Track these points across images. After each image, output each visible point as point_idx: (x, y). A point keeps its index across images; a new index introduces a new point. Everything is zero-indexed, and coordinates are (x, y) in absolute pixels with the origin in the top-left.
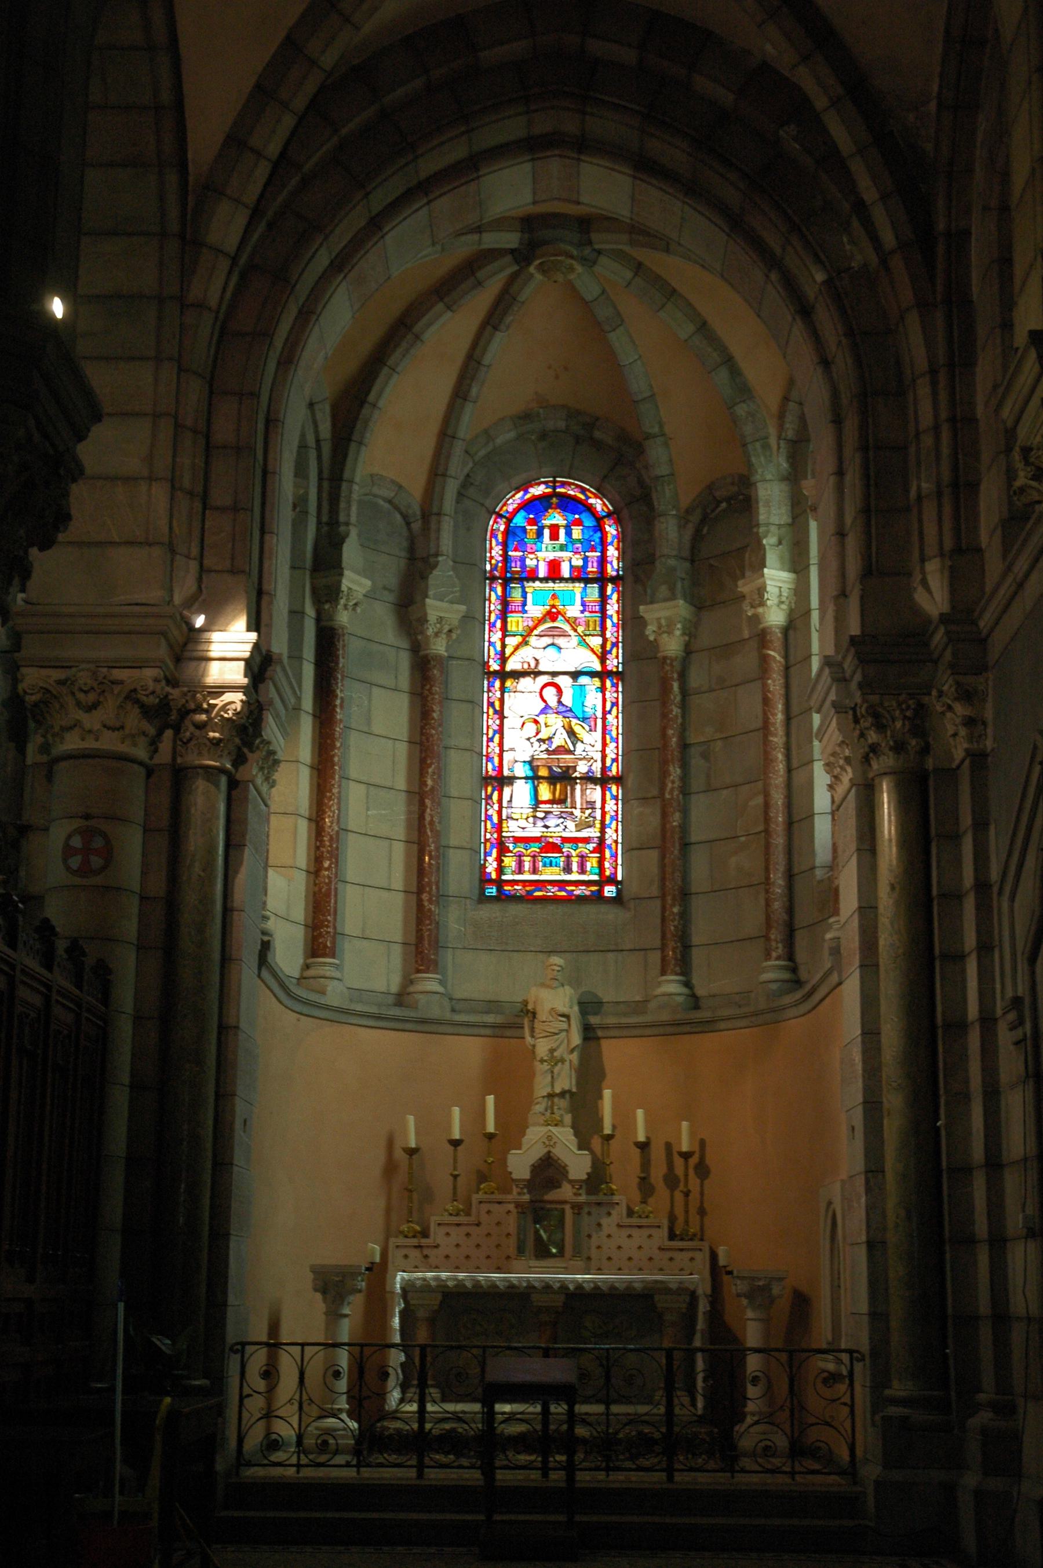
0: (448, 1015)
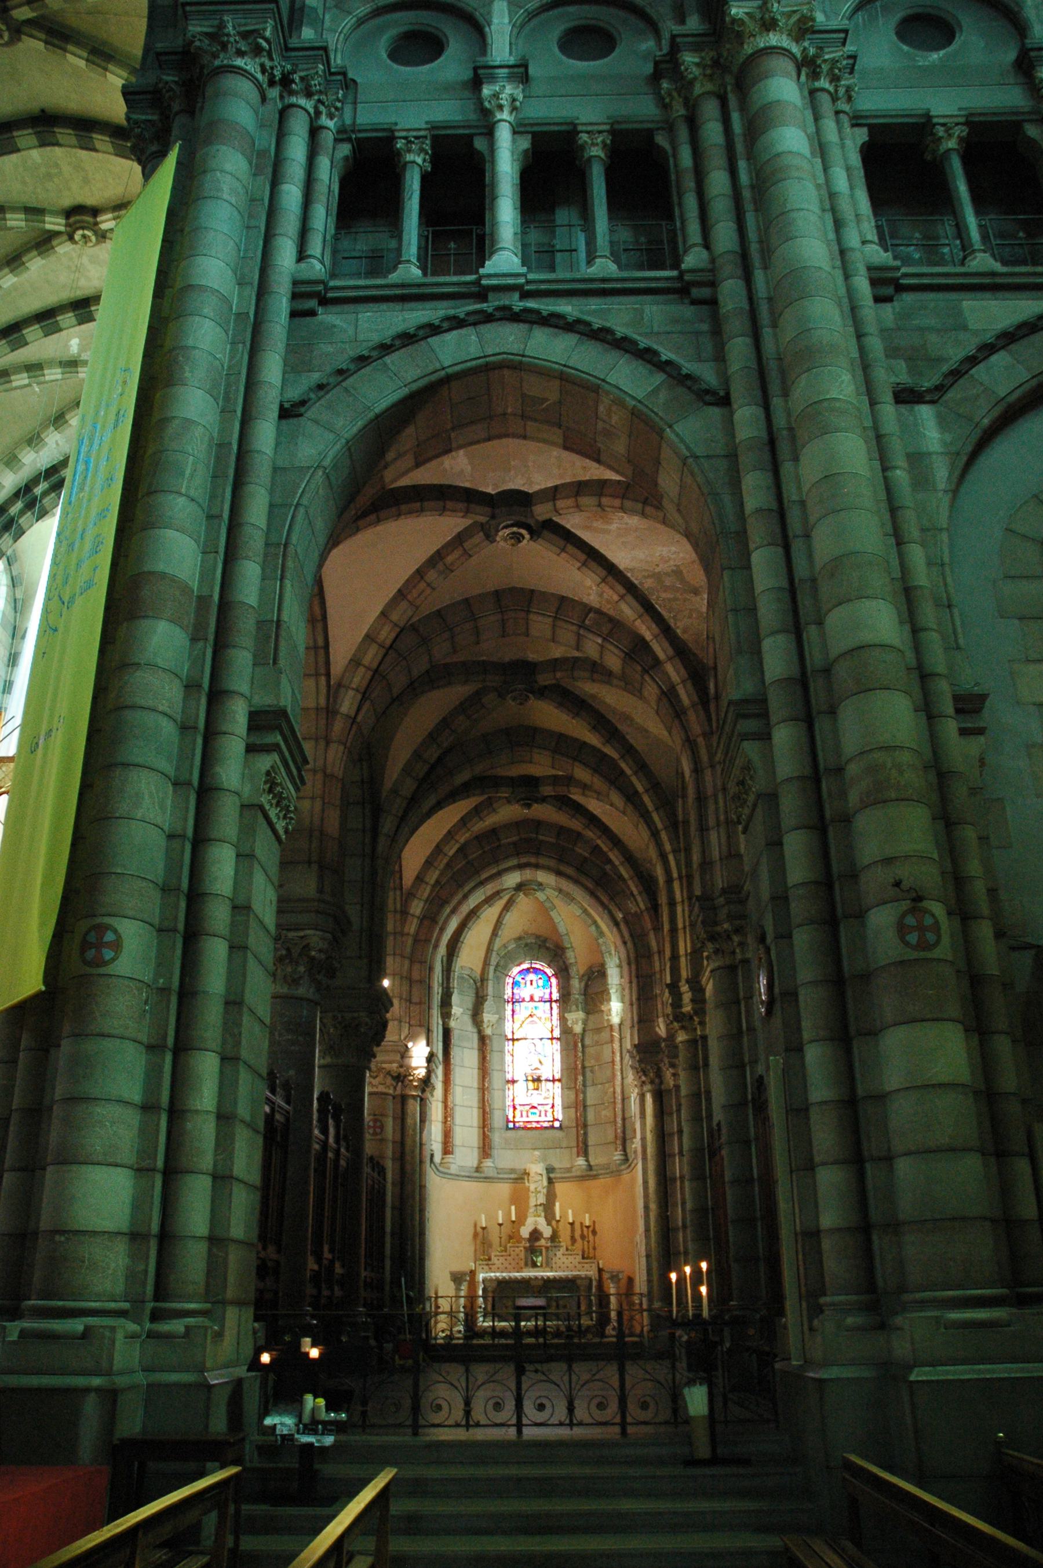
0: (496, 1175)
